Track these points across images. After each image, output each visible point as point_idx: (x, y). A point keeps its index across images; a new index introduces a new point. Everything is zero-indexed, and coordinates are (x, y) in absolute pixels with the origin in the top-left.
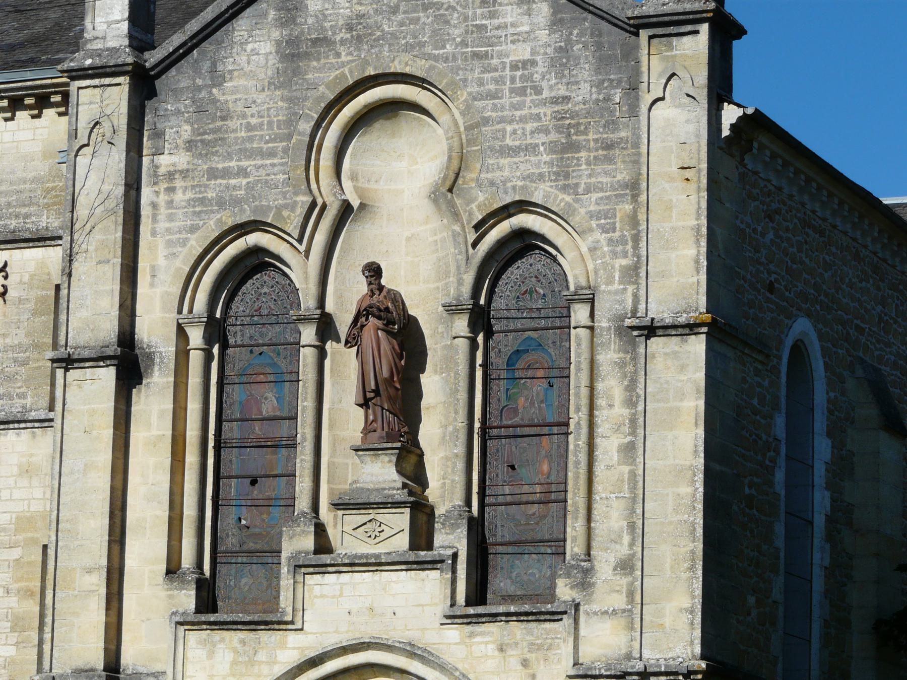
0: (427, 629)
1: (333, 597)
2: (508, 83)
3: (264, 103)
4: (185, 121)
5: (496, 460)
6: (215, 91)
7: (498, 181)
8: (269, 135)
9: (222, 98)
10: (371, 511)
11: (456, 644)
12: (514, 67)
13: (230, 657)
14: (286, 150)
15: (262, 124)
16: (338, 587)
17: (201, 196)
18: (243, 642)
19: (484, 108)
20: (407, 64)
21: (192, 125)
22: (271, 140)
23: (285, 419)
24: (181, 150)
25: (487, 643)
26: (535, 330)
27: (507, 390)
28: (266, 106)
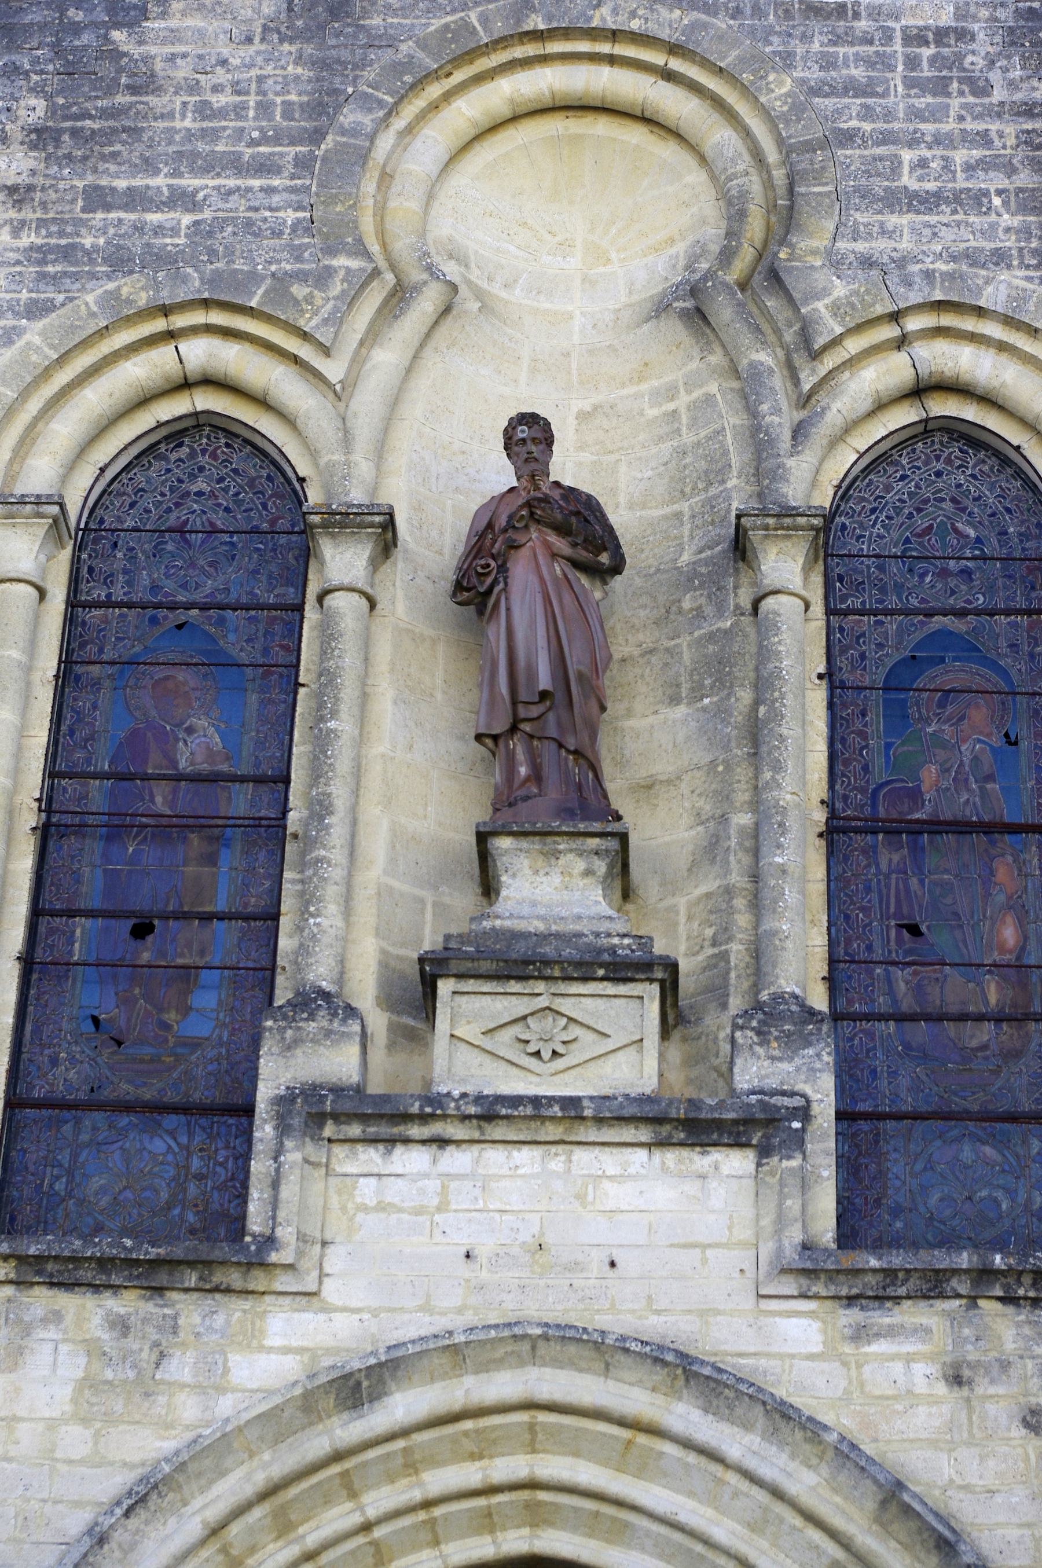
0: (719, 1312)
1: (419, 1211)
2: (900, 68)
3: (251, 66)
4: (31, 90)
5: (863, 909)
6: (116, 35)
7: (885, 259)
8: (261, 129)
9: (136, 51)
10: (540, 987)
11: (811, 1357)
12: (916, 38)
13: (73, 1365)
14: (303, 164)
15: (239, 110)
16: (433, 1185)
17: (63, 242)
18: (121, 1326)
19: (839, 112)
20: (633, 15)
21: (49, 98)
22: (264, 140)
23: (243, 779)
24: (16, 146)
25: (909, 1359)
26: (961, 613)
27: (888, 746)
28: (254, 72)
